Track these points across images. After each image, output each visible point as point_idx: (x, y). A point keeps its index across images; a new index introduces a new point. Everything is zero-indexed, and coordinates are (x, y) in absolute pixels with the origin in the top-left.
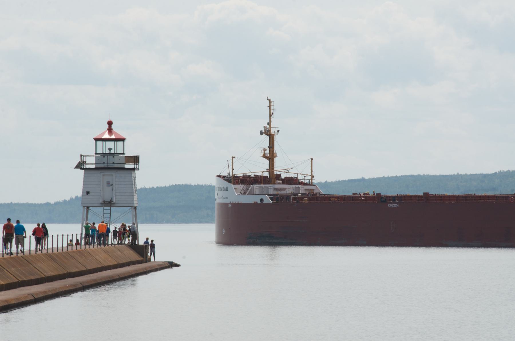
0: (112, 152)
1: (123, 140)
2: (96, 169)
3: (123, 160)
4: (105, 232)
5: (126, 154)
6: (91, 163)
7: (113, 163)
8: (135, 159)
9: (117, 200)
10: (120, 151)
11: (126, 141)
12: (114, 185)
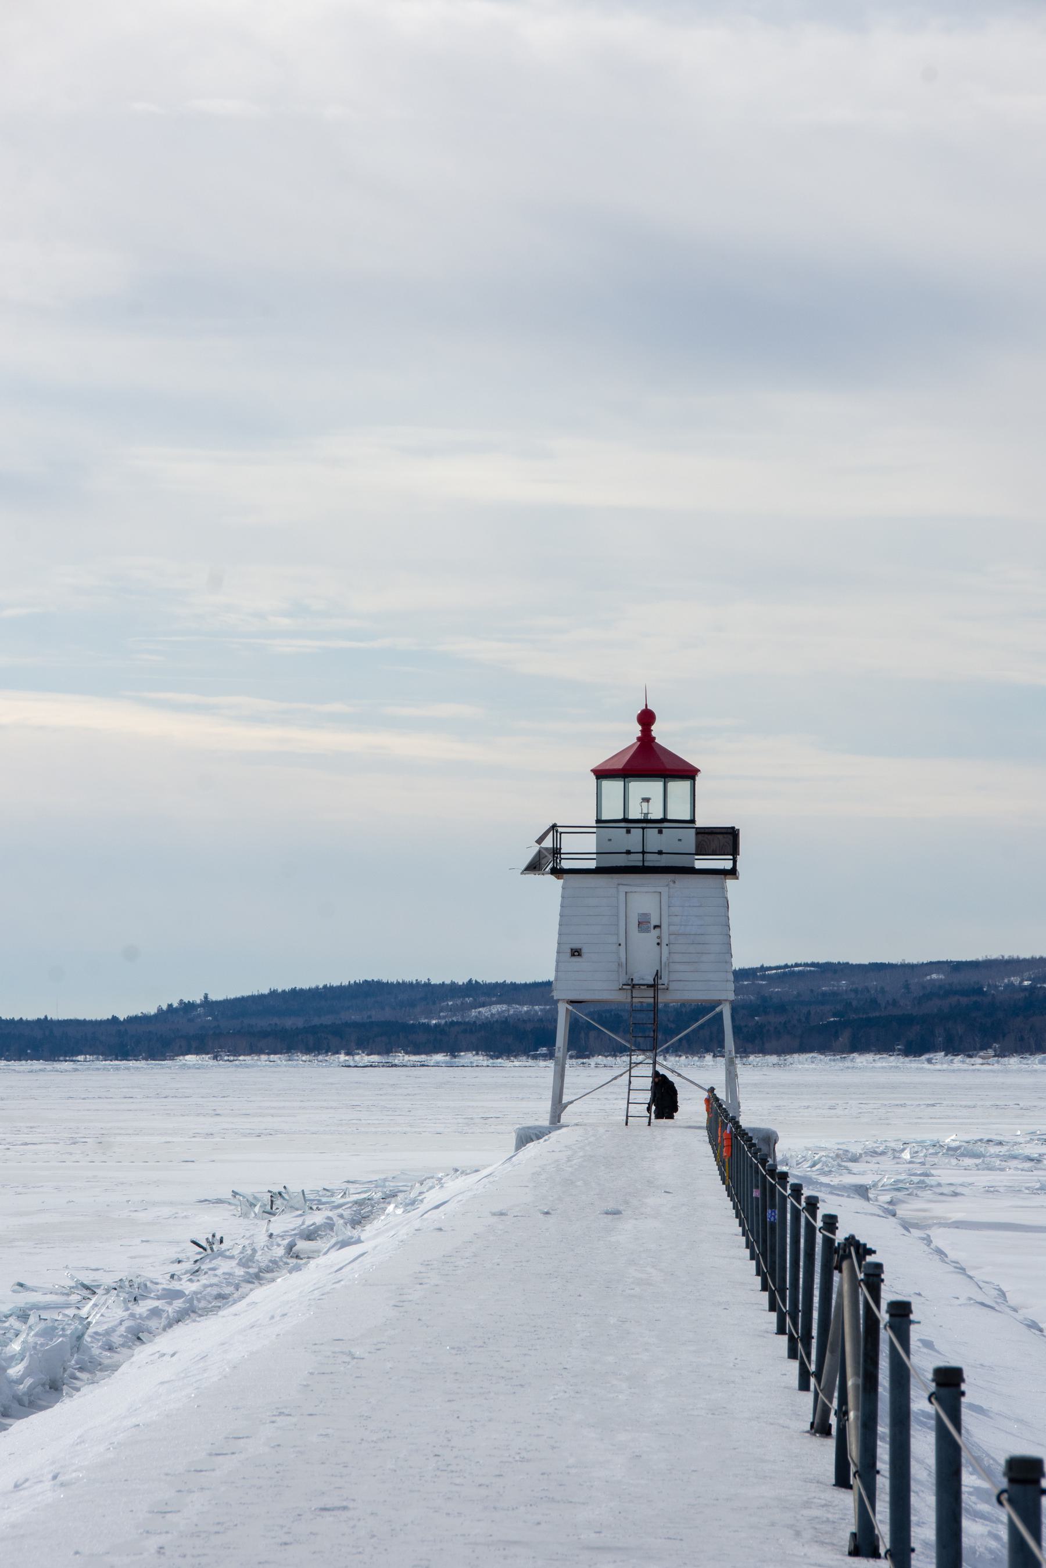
0: (656, 814)
1: (689, 773)
2: (599, 871)
3: (689, 838)
4: (738, 1061)
5: (699, 823)
6: (581, 848)
7: (660, 853)
8: (725, 840)
9: (674, 977)
10: (679, 811)
11: (699, 779)
12: (664, 926)
